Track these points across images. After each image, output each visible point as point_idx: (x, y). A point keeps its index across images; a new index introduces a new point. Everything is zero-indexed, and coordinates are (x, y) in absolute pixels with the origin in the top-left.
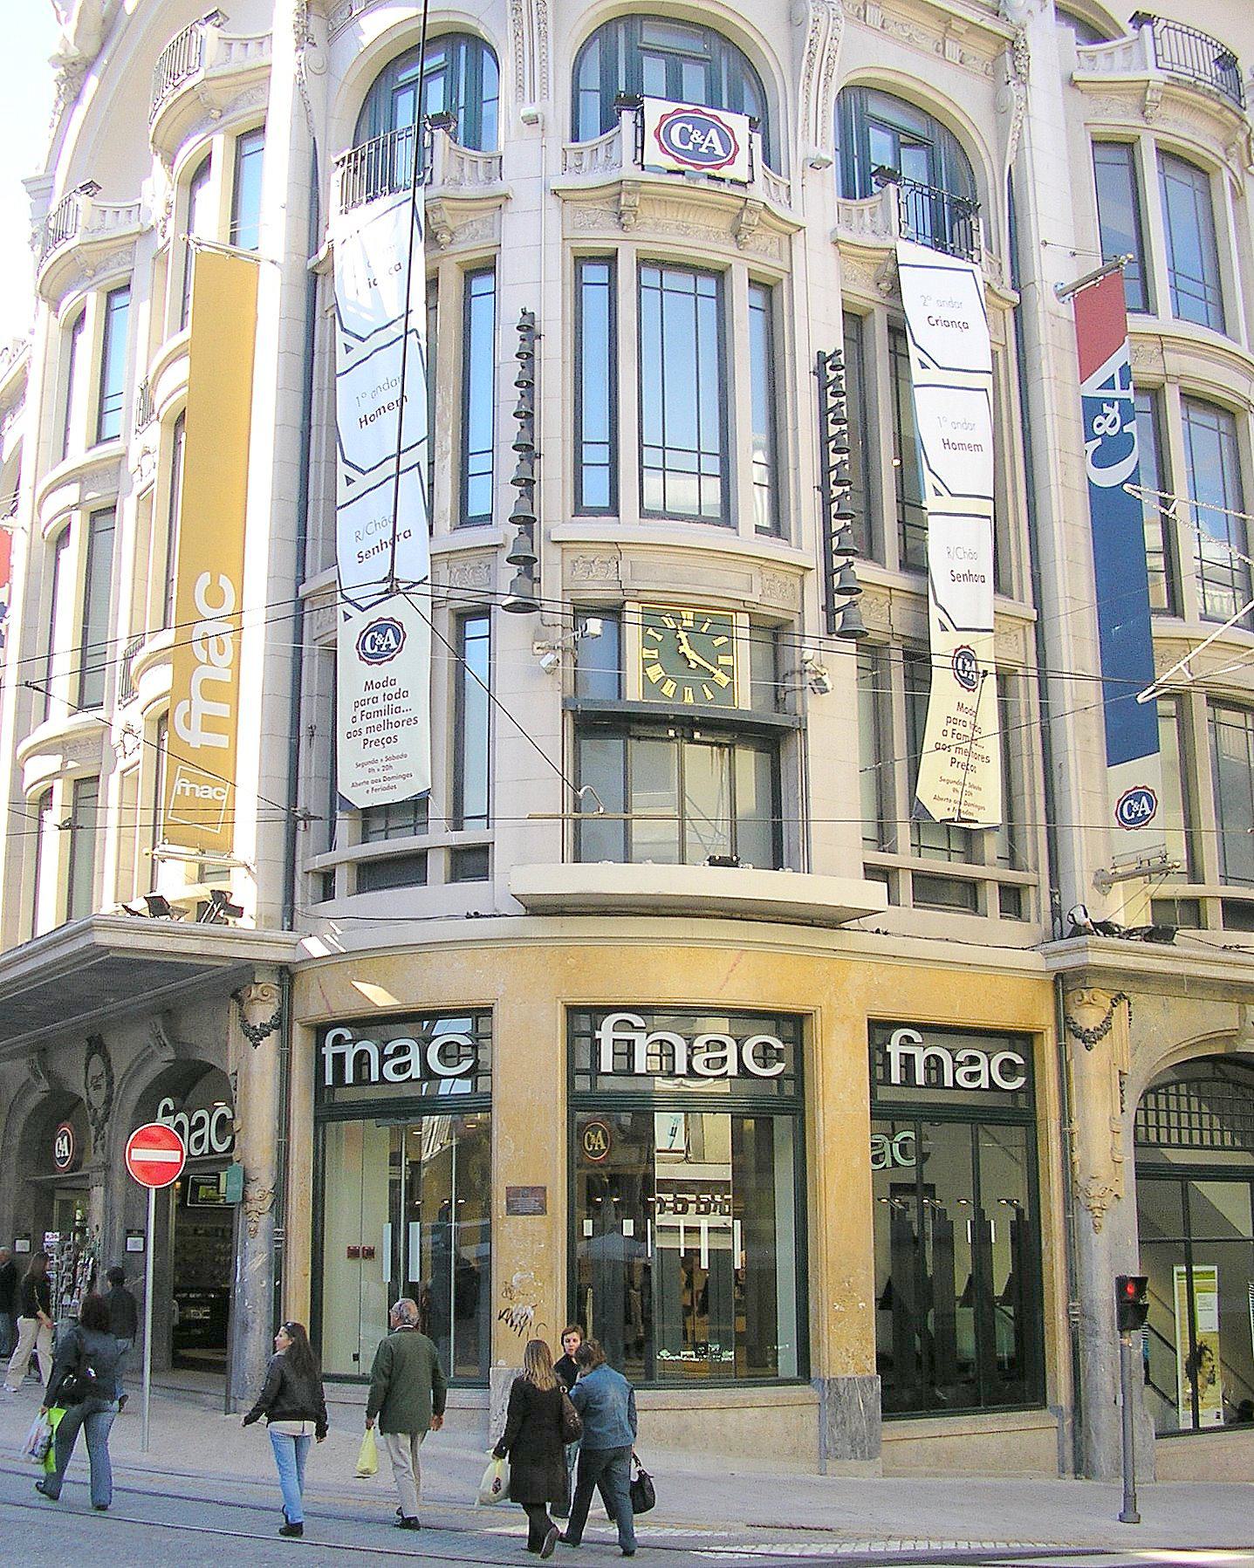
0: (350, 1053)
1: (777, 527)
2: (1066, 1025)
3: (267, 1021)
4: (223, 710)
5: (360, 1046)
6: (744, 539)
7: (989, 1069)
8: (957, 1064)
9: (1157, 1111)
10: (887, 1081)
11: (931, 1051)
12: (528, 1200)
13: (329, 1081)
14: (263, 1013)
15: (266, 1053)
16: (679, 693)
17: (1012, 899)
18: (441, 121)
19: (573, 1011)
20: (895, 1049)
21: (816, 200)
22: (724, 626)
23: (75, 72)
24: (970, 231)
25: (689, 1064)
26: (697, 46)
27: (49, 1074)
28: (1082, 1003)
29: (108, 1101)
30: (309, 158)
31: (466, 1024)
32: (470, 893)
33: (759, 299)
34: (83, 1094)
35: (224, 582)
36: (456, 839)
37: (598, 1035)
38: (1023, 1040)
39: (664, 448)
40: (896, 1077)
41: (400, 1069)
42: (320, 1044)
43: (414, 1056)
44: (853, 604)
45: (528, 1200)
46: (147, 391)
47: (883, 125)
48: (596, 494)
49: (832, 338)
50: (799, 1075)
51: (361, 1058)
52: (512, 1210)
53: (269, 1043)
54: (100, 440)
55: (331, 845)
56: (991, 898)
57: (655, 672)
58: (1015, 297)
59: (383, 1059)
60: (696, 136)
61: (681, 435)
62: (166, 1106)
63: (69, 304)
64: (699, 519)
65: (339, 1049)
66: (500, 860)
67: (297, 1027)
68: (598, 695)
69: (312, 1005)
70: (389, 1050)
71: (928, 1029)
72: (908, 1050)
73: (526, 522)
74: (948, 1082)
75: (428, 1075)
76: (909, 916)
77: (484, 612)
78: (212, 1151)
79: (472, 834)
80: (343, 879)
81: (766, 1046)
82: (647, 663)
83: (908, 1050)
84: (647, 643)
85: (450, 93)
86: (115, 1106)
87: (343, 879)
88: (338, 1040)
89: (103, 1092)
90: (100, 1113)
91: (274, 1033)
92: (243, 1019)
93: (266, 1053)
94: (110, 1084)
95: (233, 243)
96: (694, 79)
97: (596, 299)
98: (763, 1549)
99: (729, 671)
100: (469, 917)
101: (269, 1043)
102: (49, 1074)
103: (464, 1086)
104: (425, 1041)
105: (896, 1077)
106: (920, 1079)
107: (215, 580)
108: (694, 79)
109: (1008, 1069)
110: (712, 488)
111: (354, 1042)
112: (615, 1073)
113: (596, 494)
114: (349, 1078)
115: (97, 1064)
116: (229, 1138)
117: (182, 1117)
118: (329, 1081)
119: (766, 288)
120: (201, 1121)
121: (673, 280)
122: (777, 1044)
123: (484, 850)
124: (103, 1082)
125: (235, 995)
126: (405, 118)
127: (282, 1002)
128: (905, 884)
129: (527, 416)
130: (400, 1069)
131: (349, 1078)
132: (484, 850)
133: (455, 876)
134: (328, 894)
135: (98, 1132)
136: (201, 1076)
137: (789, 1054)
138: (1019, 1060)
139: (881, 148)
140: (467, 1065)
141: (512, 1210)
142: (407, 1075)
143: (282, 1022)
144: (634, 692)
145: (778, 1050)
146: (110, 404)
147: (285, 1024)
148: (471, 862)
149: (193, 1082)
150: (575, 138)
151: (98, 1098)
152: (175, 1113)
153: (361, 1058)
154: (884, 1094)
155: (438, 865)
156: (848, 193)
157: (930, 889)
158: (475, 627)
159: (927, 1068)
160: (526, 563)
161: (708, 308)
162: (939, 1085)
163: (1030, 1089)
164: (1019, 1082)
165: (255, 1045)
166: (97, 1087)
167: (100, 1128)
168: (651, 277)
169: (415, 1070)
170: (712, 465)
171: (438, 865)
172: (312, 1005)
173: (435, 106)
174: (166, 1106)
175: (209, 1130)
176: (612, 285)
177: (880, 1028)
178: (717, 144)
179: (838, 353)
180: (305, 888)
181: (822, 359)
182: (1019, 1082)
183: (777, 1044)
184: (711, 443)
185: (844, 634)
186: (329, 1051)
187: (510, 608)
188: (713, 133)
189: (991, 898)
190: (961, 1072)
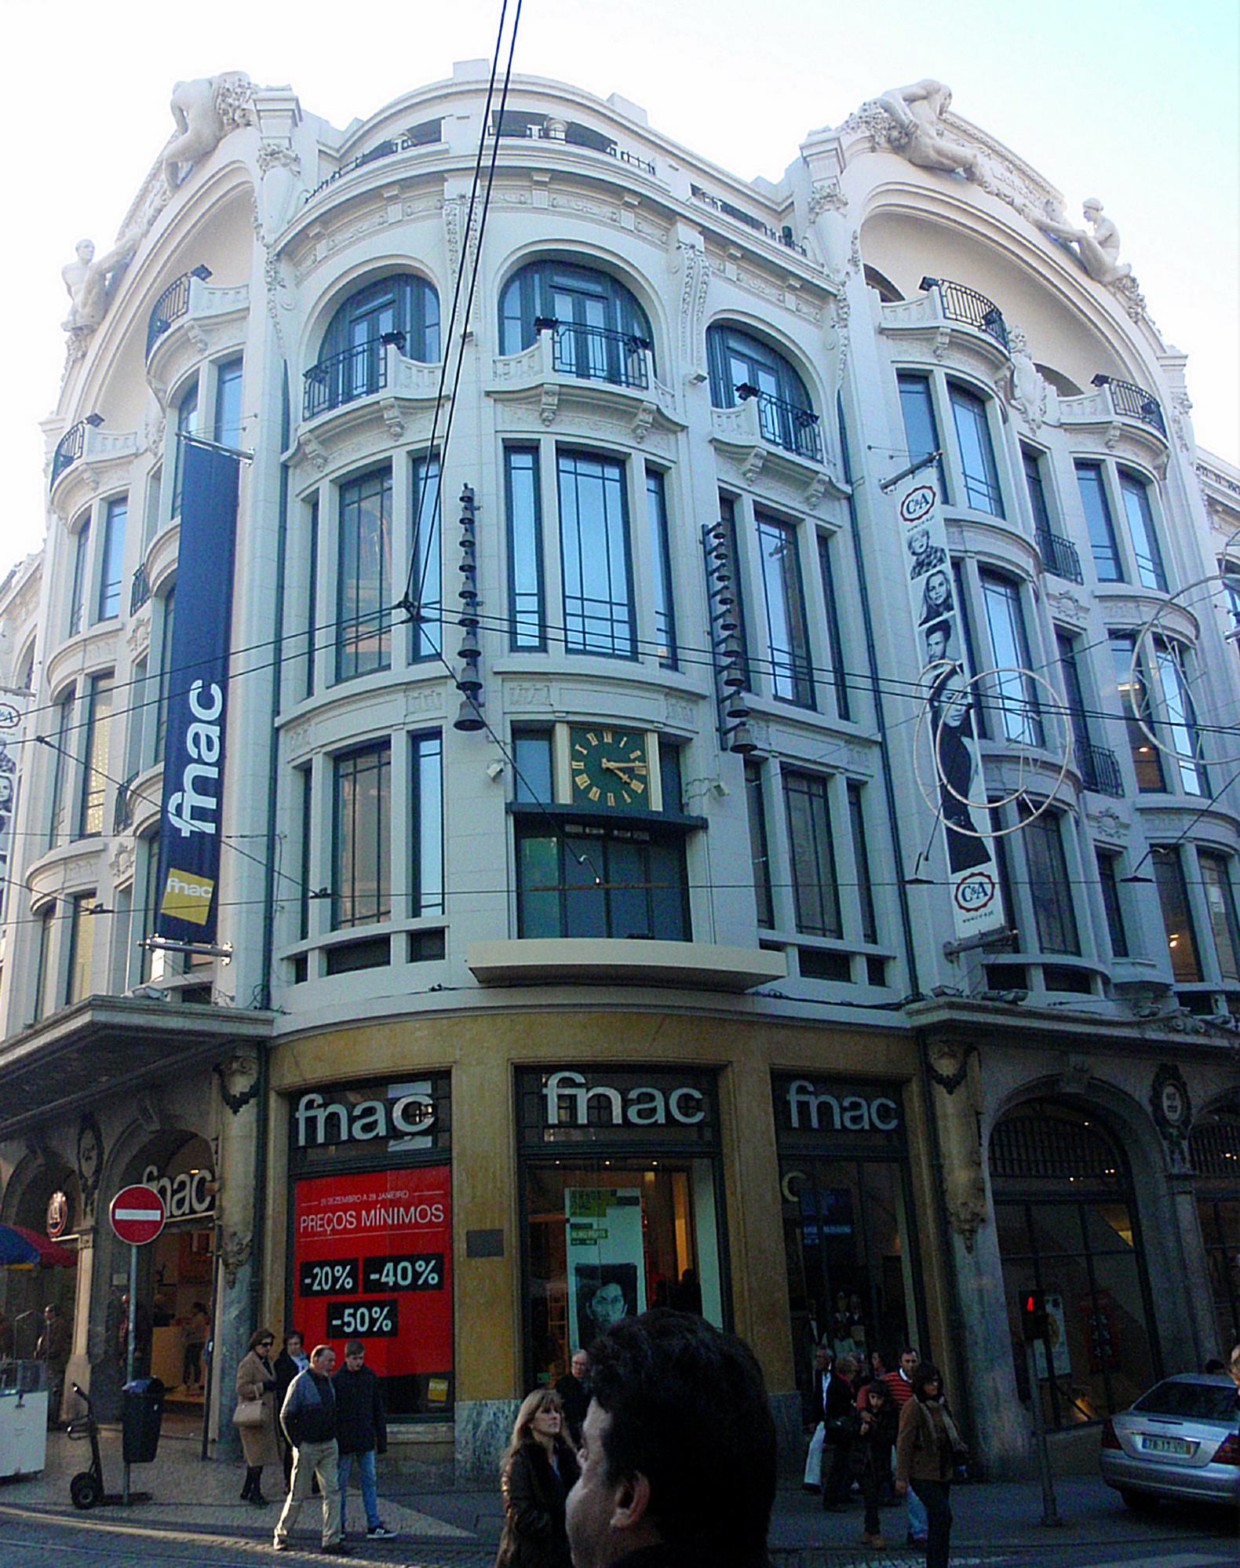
0: (322, 1115)
1: (673, 663)
2: (930, 1074)
3: (247, 1090)
4: (210, 803)
5: (332, 1108)
6: (650, 670)
7: (869, 1113)
8: (843, 1110)
9: (1009, 1146)
11: (823, 1098)
12: (484, 1244)
13: (302, 1142)
14: (240, 1085)
15: (239, 1125)
16: (603, 796)
17: (877, 968)
18: (388, 339)
20: (793, 1098)
21: (695, 409)
23: (81, 332)
24: (814, 437)
27: (46, 1150)
29: (97, 1171)
30: (279, 383)
31: (426, 1087)
32: (428, 971)
33: (652, 484)
34: (76, 1167)
35: (215, 690)
36: (416, 924)
37: (545, 1091)
38: (893, 1086)
39: (582, 599)
40: (795, 1123)
41: (367, 1128)
42: (294, 1108)
43: (380, 1115)
44: (743, 724)
45: (484, 1244)
46: (141, 576)
47: (742, 356)
48: (528, 633)
49: (713, 515)
50: (714, 1124)
51: (332, 1120)
53: (248, 1112)
54: (101, 619)
55: (304, 935)
57: (583, 781)
59: (352, 1120)
61: (595, 587)
62: (151, 1173)
63: (74, 510)
64: (613, 655)
65: (311, 1113)
67: (273, 1101)
68: (535, 796)
69: (287, 1076)
70: (357, 1112)
72: (804, 1098)
73: (471, 655)
75: (394, 1133)
77: (435, 734)
78: (192, 1211)
79: (430, 918)
80: (314, 963)
82: (575, 773)
83: (804, 1098)
84: (575, 756)
85: (398, 320)
86: (104, 1174)
87: (314, 963)
88: (310, 1105)
89: (94, 1163)
90: (90, 1183)
91: (252, 1101)
92: (224, 1089)
93: (239, 1125)
94: (100, 1155)
95: (216, 440)
97: (523, 481)
99: (644, 779)
100: (433, 990)
101: (248, 1112)
102: (46, 1150)
103: (427, 1142)
104: (390, 1104)
105: (795, 1123)
106: (815, 1123)
107: (206, 688)
110: (623, 630)
111: (325, 1105)
113: (528, 633)
114: (321, 1139)
115: (88, 1140)
116: (208, 1199)
117: (165, 1182)
118: (302, 1142)
119: (656, 473)
120: (182, 1185)
122: (697, 1095)
123: (438, 933)
124: (94, 1154)
125: (217, 1069)
126: (361, 333)
127: (260, 1073)
129: (469, 569)
130: (367, 1128)
131: (321, 1139)
132: (438, 933)
133: (415, 956)
134: (301, 976)
135: (87, 1198)
136: (187, 1141)
137: (706, 1105)
140: (429, 1121)
141: (471, 1253)
142: (374, 1133)
143: (258, 1092)
144: (565, 797)
145: (698, 1100)
146: (111, 591)
147: (262, 1092)
148: (427, 944)
149: (178, 1149)
150: (502, 352)
151: (88, 1168)
152: (159, 1178)
153: (332, 1120)
155: (399, 947)
156: (716, 403)
158: (427, 747)
160: (471, 688)
161: (614, 488)
163: (902, 1130)
164: (893, 1124)
165: (235, 1112)
166: (89, 1158)
167: (89, 1196)
168: (567, 464)
169: (381, 1129)
170: (622, 613)
171: (399, 947)
172: (287, 1076)
173: (386, 326)
174: (151, 1173)
175: (190, 1192)
176: (536, 469)
177: (527, 1077)
179: (719, 524)
180: (282, 972)
183: (697, 1095)
184: (620, 594)
185: (736, 749)
186: (302, 1115)
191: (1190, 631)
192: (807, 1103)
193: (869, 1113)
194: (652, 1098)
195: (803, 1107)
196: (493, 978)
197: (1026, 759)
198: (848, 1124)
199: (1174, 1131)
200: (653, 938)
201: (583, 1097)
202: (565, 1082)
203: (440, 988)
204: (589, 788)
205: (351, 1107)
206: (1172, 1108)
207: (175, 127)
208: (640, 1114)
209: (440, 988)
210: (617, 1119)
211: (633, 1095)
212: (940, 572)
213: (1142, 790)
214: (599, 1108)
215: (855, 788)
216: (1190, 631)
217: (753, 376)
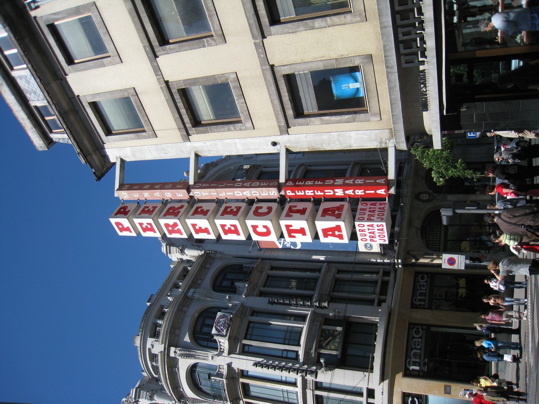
7: (422, 282)
8: (421, 289)
10: (424, 305)
19: (410, 324)
20: (417, 303)
22: (323, 331)
24: (246, 267)
25: (418, 349)
26: (201, 320)
28: (485, 379)
32: (377, 394)
38: (417, 274)
40: (423, 303)
47: (222, 282)
49: (265, 300)
52: (445, 386)
56: (386, 278)
58: (260, 260)
60: (221, 323)
66: (371, 387)
71: (414, 295)
74: (424, 292)
76: (389, 298)
81: (415, 332)
96: (208, 322)
98: (530, 350)
104: (414, 338)
108: (208, 322)
109: (423, 278)
112: (420, 358)
121: (249, 332)
128: (383, 297)
133: (373, 397)
137: (417, 327)
138: (420, 276)
139: (225, 283)
154: (426, 306)
157: (384, 291)
159: (421, 296)
161: (256, 325)
162: (425, 294)
164: (425, 276)
168: (248, 337)
177: (408, 374)
178: (223, 319)
181: (269, 302)
182: (425, 276)
183: (415, 329)
187: (316, 378)
188: (221, 320)
189: (386, 278)
190: (423, 289)
191: (303, 167)
192: (413, 362)
193: (422, 282)
194: (415, 341)
195: (420, 300)
196: (382, 379)
197: (385, 57)
198: (424, 289)
199: (432, 197)
200: (295, 8)
201: (419, 297)
202: (415, 300)
203: (382, 393)
204: (335, 346)
205: (412, 349)
206: (426, 197)
207: (389, 136)
208: (419, 345)
209: (382, 393)
210: (419, 351)
211: (414, 346)
212: (226, 336)
213: (404, 49)
214: (416, 355)
215: (339, 271)
216: (303, 167)
217: (228, 280)
